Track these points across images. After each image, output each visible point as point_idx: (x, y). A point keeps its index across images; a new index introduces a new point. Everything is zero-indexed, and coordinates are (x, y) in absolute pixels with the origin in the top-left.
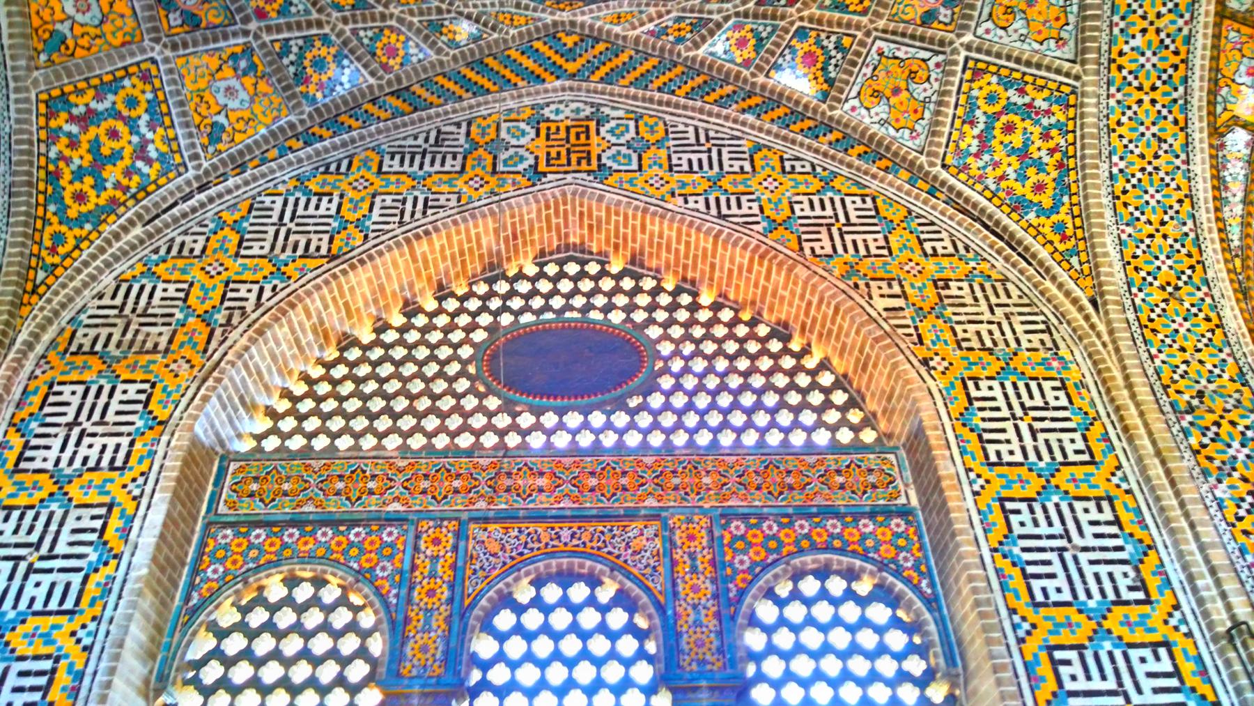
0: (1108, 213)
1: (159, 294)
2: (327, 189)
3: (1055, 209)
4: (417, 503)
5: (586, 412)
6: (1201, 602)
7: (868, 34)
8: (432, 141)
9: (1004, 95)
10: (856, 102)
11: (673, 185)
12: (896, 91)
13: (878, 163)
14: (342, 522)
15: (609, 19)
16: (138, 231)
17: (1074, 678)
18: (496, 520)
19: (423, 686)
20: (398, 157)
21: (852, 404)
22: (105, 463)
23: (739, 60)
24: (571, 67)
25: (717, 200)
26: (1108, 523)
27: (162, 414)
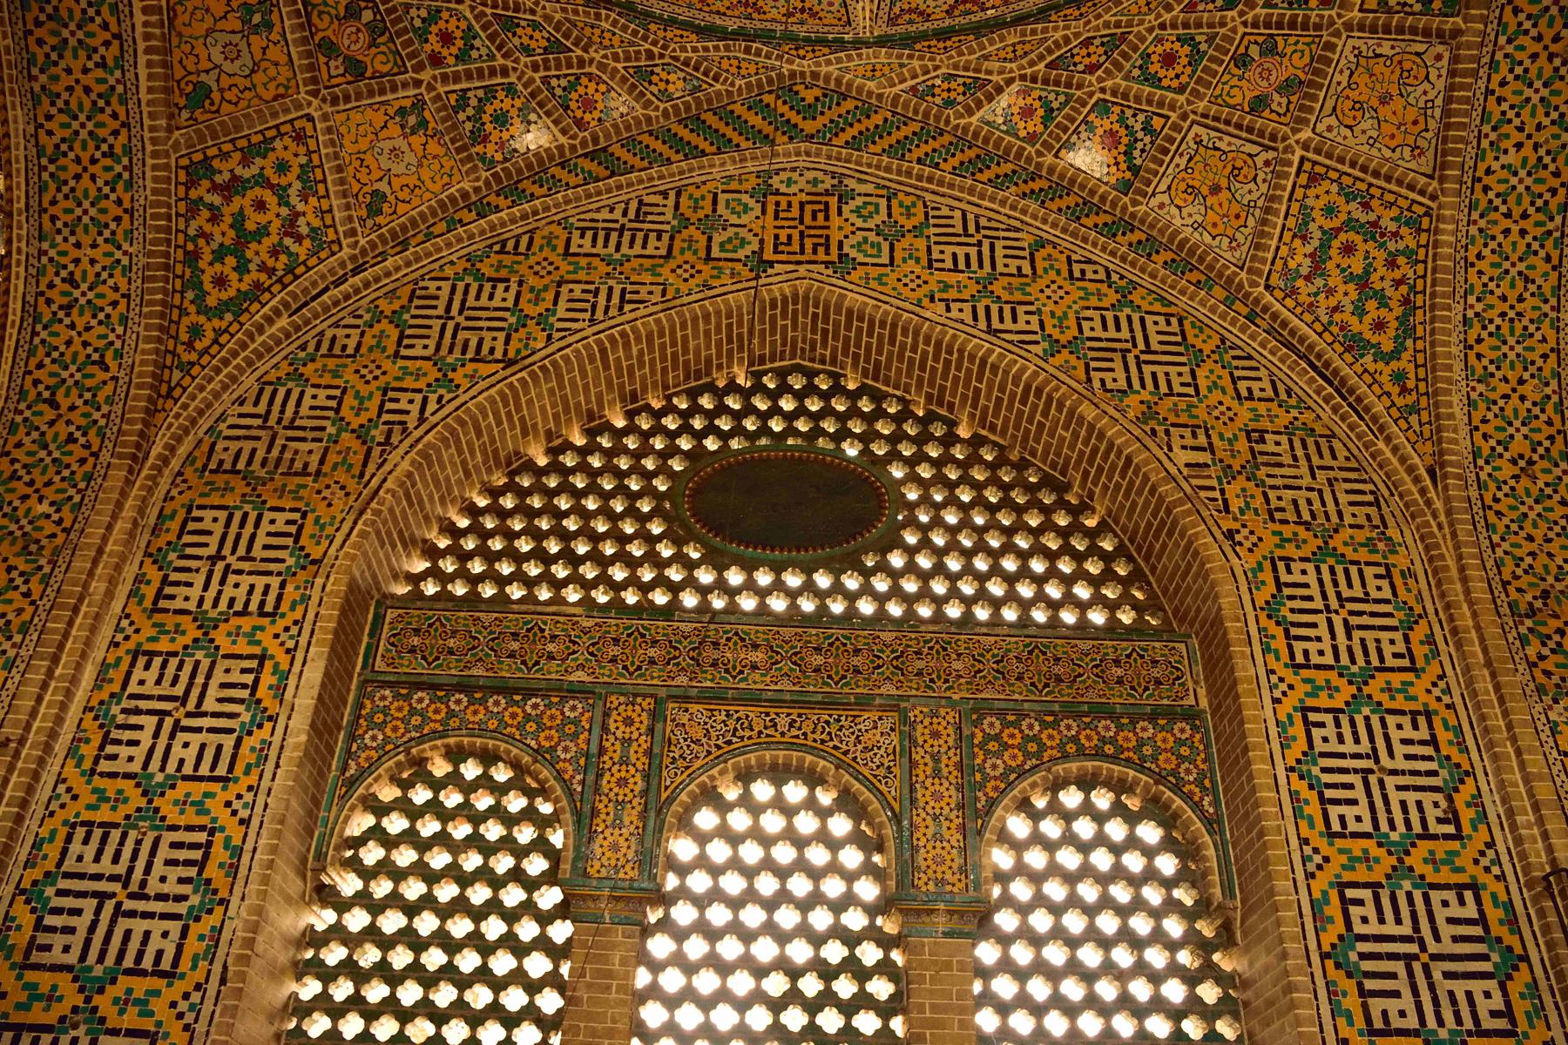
0: (1458, 366)
1: (307, 401)
2: (503, 273)
3: (1395, 354)
4: (606, 673)
5: (809, 571)
6: (1519, 841)
7: (1184, 117)
8: (632, 215)
9: (1344, 208)
10: (1165, 198)
11: (933, 286)
12: (1216, 189)
13: (1188, 275)
14: (516, 691)
15: (861, 71)
16: (283, 322)
17: (1365, 920)
18: (698, 700)
19: (613, 889)
20: (589, 234)
21: (1136, 577)
22: (253, 607)
23: (1023, 134)
24: (809, 127)
25: (987, 308)
26: (1422, 743)
27: (316, 553)
